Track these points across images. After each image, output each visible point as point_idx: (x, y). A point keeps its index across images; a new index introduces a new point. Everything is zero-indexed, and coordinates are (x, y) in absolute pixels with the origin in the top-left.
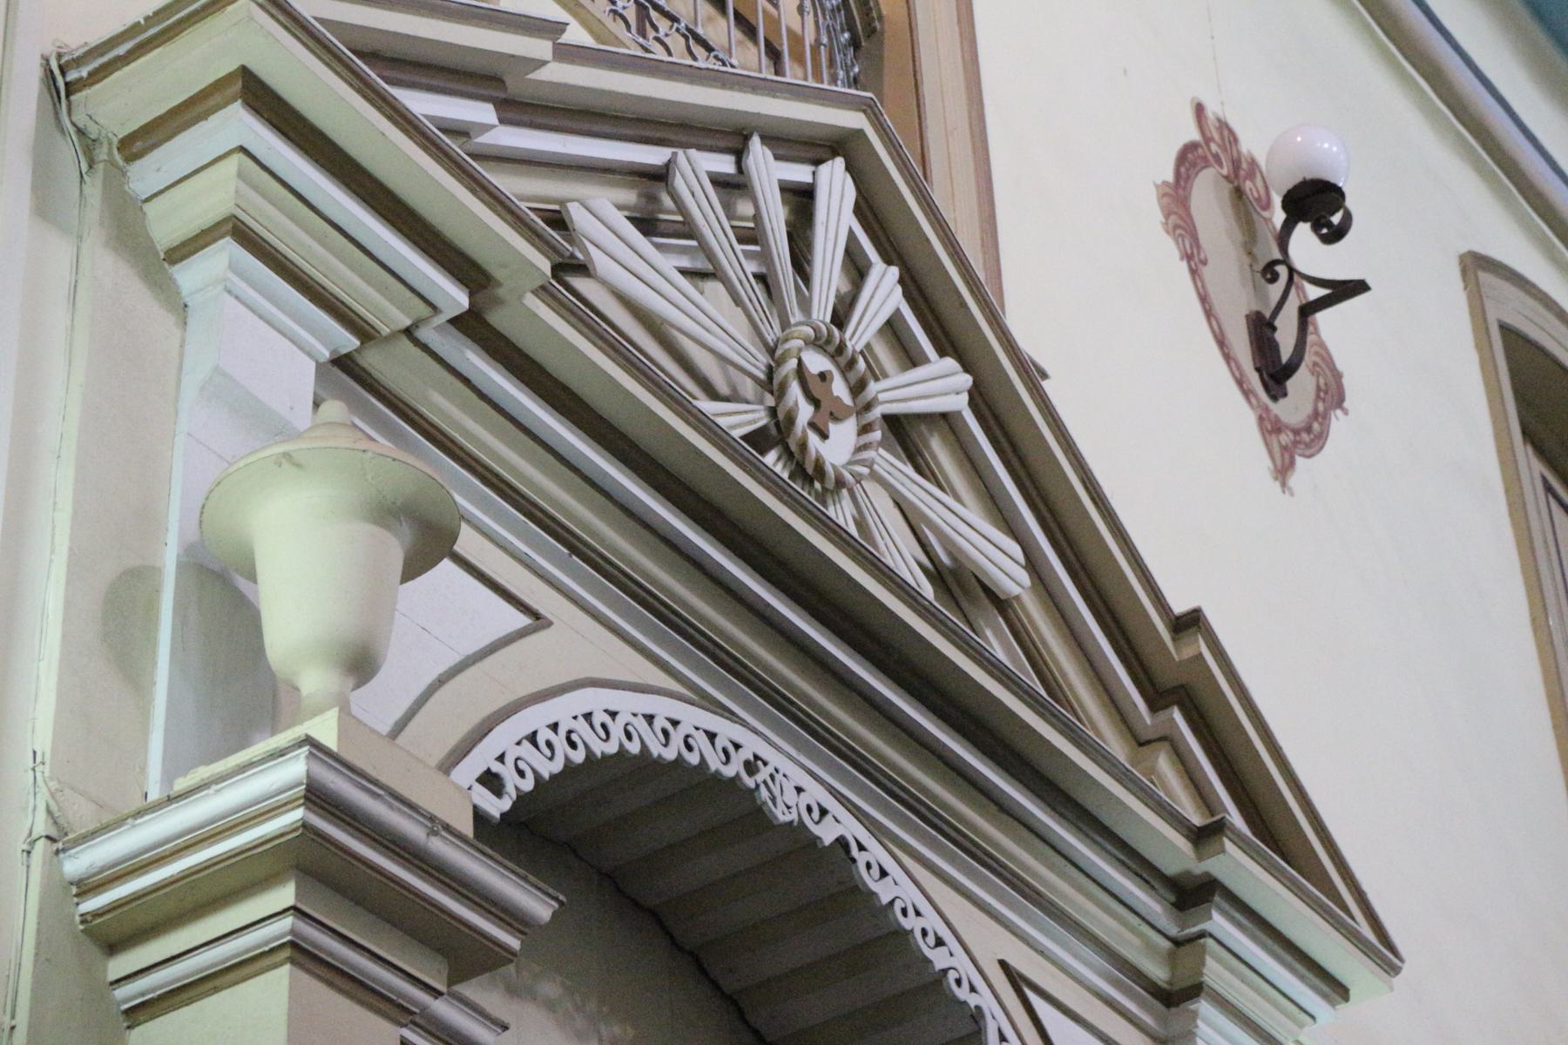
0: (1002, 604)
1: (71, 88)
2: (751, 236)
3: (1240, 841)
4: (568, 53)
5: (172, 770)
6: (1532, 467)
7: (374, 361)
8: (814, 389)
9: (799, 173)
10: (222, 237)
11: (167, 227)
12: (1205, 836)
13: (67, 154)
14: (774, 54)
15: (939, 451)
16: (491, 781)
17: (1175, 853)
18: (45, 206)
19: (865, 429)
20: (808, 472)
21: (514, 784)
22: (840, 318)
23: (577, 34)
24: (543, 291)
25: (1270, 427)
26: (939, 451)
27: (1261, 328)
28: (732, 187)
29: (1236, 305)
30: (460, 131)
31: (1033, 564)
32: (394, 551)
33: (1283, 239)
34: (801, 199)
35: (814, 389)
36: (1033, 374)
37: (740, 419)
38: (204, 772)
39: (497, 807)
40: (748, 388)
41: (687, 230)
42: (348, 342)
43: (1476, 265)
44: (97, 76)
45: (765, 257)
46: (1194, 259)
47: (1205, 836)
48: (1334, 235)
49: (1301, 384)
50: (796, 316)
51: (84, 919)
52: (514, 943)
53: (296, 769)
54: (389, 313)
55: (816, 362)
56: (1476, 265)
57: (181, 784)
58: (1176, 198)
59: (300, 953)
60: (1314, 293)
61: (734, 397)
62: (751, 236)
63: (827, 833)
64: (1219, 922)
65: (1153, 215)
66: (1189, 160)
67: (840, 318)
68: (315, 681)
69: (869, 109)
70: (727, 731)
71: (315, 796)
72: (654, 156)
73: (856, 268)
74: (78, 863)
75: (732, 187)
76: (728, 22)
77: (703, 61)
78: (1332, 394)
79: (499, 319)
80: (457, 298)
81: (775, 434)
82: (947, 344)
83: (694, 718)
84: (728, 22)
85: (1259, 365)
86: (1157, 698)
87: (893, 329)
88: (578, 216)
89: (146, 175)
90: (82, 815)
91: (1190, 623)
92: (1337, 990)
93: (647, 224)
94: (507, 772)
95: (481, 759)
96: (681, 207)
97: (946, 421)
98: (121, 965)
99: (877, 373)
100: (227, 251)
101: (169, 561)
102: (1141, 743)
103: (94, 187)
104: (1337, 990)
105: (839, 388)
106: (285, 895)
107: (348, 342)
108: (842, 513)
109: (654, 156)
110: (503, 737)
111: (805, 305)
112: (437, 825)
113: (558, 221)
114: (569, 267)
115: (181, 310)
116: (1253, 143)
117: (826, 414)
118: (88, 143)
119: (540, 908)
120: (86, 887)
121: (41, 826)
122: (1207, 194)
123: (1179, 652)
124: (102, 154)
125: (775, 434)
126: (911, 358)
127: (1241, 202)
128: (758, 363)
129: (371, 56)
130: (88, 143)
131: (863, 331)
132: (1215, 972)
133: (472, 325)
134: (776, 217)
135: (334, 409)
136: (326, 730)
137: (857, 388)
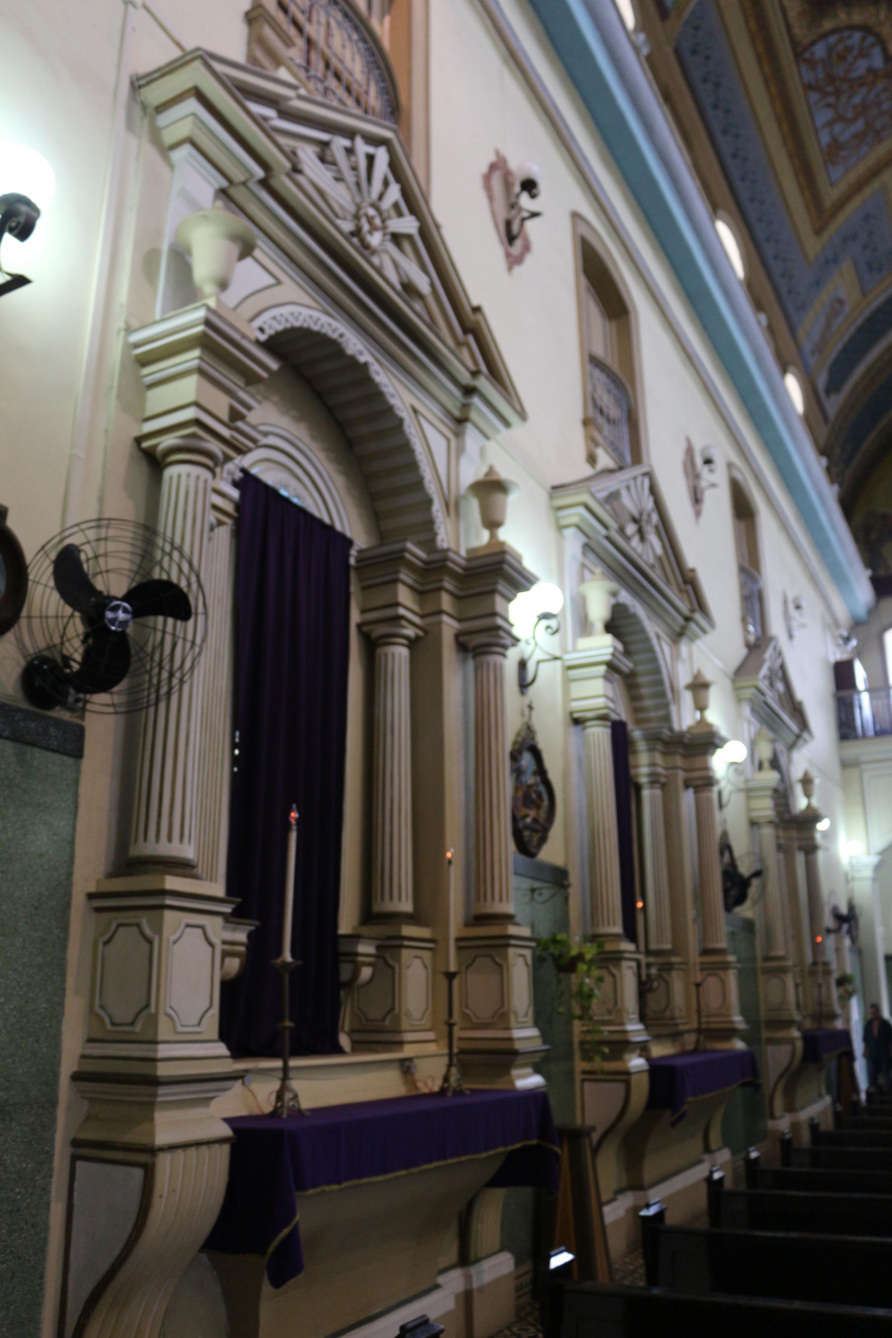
0: (421, 297)
1: (140, 87)
2: (355, 168)
3: (486, 377)
4: (300, 97)
5: (164, 311)
6: (584, 281)
7: (233, 192)
8: (370, 220)
9: (370, 150)
10: (189, 97)
11: (169, 137)
12: (475, 374)
13: (137, 110)
14: (366, 112)
15: (407, 246)
16: (262, 330)
17: (465, 377)
18: (130, 125)
19: (384, 235)
20: (366, 246)
21: (270, 332)
22: (381, 197)
23: (302, 92)
24: (288, 175)
25: (508, 255)
26: (407, 246)
27: (508, 224)
28: (350, 151)
29: (502, 215)
30: (265, 119)
31: (432, 285)
32: (236, 250)
33: (518, 196)
34: (371, 159)
35: (370, 220)
36: (438, 227)
37: (347, 226)
38: (173, 313)
39: (263, 338)
40: (349, 217)
41: (334, 163)
42: (224, 183)
43: (576, 216)
44: (148, 83)
45: (358, 176)
46: (491, 198)
47: (475, 374)
48: (533, 196)
49: (518, 243)
50: (366, 195)
51: (137, 356)
52: (264, 375)
53: (201, 314)
54: (238, 176)
55: (371, 212)
56: (576, 216)
57: (166, 316)
58: (487, 179)
59: (200, 371)
60: (526, 214)
61: (345, 219)
62: (355, 168)
63: (362, 359)
64: (476, 401)
65: (479, 183)
66: (493, 167)
67: (381, 197)
68: (209, 289)
69: (394, 131)
70: (335, 324)
71: (208, 323)
72: (324, 136)
73: (386, 183)
74: (135, 338)
75: (350, 151)
76: (193, 1026)
77: (342, 107)
78: (527, 248)
79: (274, 182)
80: (260, 173)
81: (357, 233)
82: (414, 210)
83: (325, 319)
84: (193, 1026)
85: (479, 317)
86: (466, 330)
87: (396, 206)
88: (300, 153)
89: (163, 119)
90: (135, 324)
91: (477, 310)
92: (507, 424)
93: (322, 159)
94: (266, 327)
95: (257, 323)
96: (333, 156)
97: (409, 237)
98: (146, 371)
99: (389, 218)
100: (187, 149)
101: (165, 247)
102: (459, 344)
103: (146, 122)
104: (507, 424)
105: (378, 221)
106: (196, 353)
107: (224, 183)
108: (376, 260)
109: (324, 136)
110: (266, 316)
111: (369, 193)
112: (244, 336)
113: (294, 153)
114: (296, 169)
115: (171, 166)
116: (514, 164)
117: (373, 229)
118: (144, 107)
119: (274, 365)
120: (136, 346)
121: (122, 325)
122: (497, 182)
123: (472, 317)
124: (149, 111)
125: (357, 233)
126: (400, 214)
127: (507, 184)
128: (352, 209)
129: (240, 89)
130: (144, 107)
131: (387, 204)
132: (473, 415)
133: (264, 183)
134: (363, 164)
135: (220, 204)
136: (212, 302)
137: (383, 221)
